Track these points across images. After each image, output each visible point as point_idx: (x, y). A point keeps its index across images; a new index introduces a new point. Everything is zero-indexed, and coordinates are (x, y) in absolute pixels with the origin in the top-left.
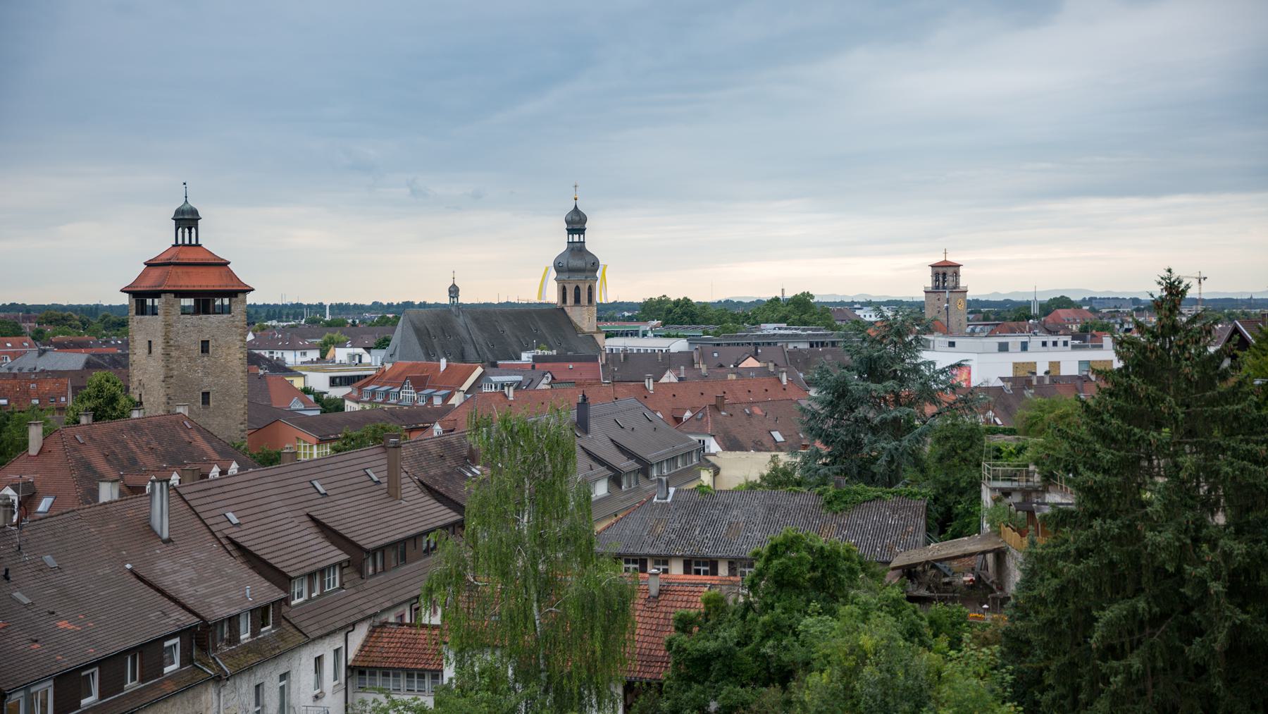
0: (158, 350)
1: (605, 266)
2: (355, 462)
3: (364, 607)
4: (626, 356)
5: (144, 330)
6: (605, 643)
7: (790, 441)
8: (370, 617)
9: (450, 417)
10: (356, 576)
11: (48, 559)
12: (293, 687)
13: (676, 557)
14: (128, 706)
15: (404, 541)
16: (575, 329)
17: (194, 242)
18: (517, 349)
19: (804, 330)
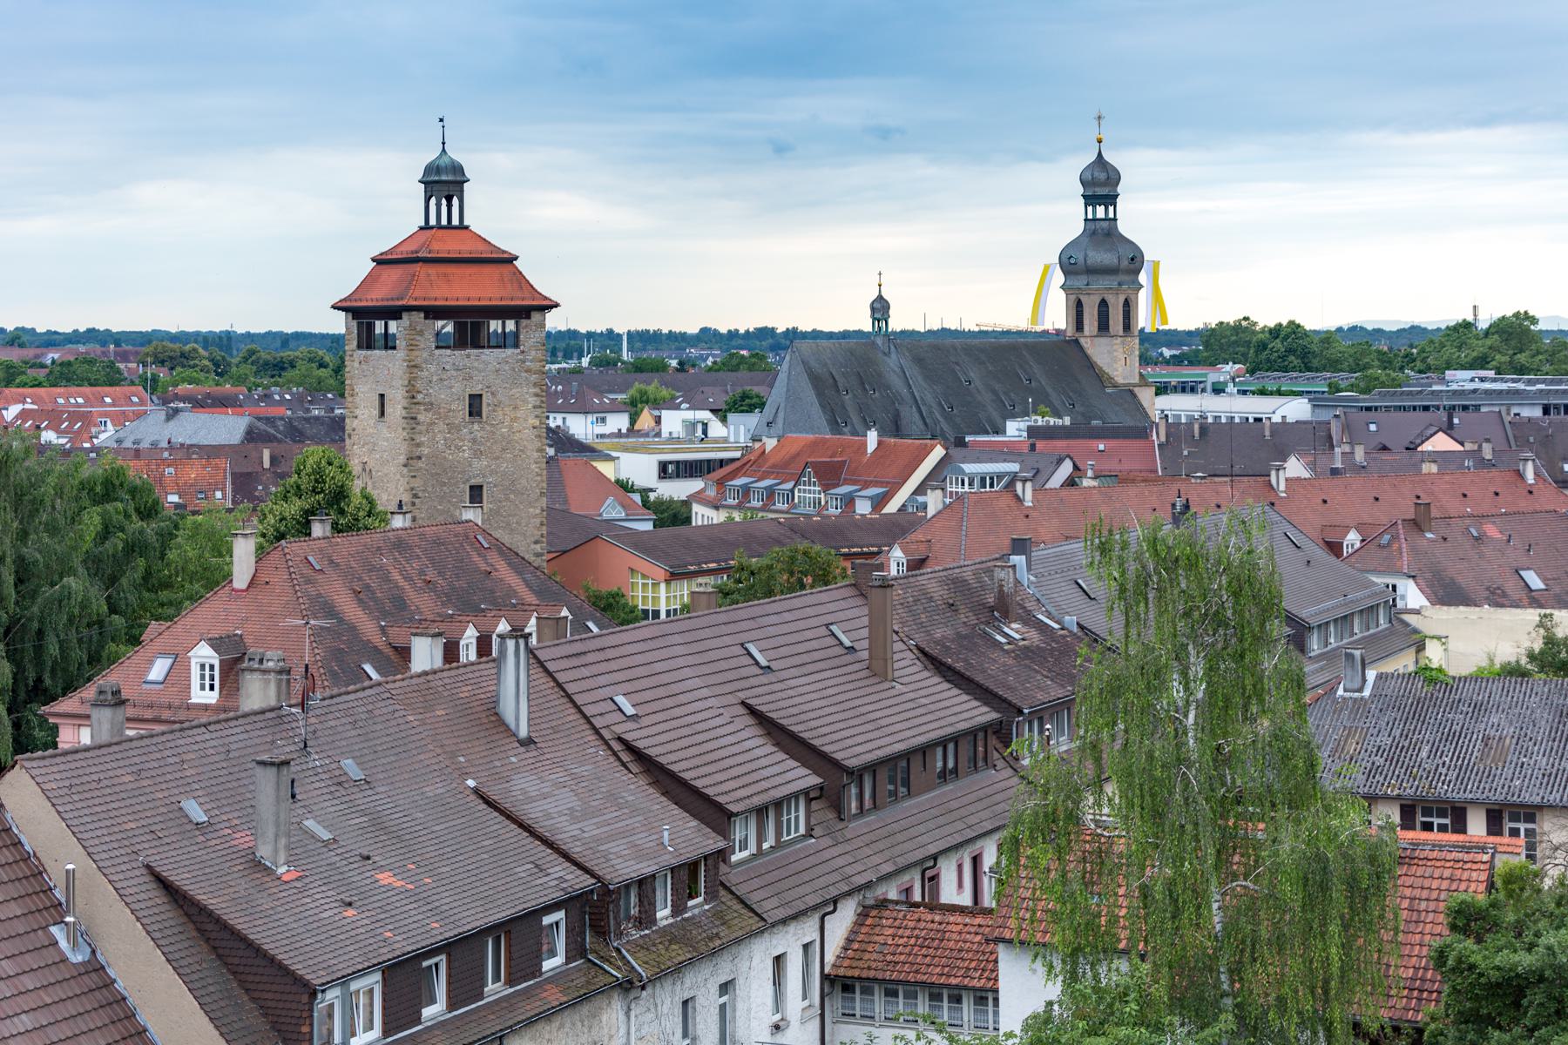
0: (396, 410)
1: (1156, 264)
2: (810, 611)
3: (849, 870)
4: (1204, 429)
5: (373, 378)
6: (1346, 947)
7: (1557, 590)
8: (859, 889)
9: (919, 535)
10: (831, 815)
11: (348, 764)
12: (741, 1006)
13: (1386, 798)
14: (492, 1026)
15: (907, 755)
16: (1100, 378)
17: (455, 222)
18: (995, 415)
19: (1529, 382)
